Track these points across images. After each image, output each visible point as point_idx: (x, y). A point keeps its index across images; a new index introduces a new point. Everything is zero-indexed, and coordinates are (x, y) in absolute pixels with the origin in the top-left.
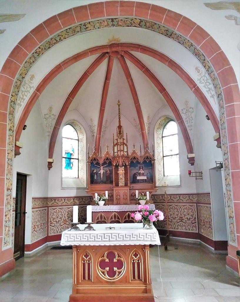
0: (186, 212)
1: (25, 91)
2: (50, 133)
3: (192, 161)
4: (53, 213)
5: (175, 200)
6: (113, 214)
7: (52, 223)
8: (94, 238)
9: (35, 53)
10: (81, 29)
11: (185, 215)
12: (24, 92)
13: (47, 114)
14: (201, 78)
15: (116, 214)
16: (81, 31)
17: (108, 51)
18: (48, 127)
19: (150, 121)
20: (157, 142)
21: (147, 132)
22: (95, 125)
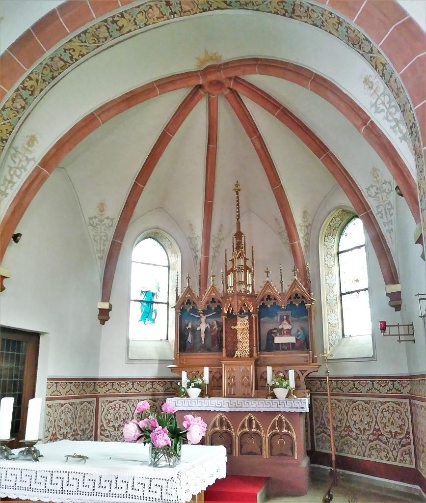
0: (387, 418)
1: (17, 168)
2: (103, 253)
3: (396, 300)
4: (108, 410)
5: (364, 390)
6: (218, 416)
7: (105, 430)
8: (28, 482)
9: (21, 90)
10: (109, 32)
11: (385, 426)
12: (14, 169)
13: (95, 217)
14: (376, 102)
15: (224, 416)
16: (111, 36)
17: (201, 83)
18: (99, 241)
19: (310, 221)
20: (325, 264)
21: (302, 244)
22: (198, 236)
